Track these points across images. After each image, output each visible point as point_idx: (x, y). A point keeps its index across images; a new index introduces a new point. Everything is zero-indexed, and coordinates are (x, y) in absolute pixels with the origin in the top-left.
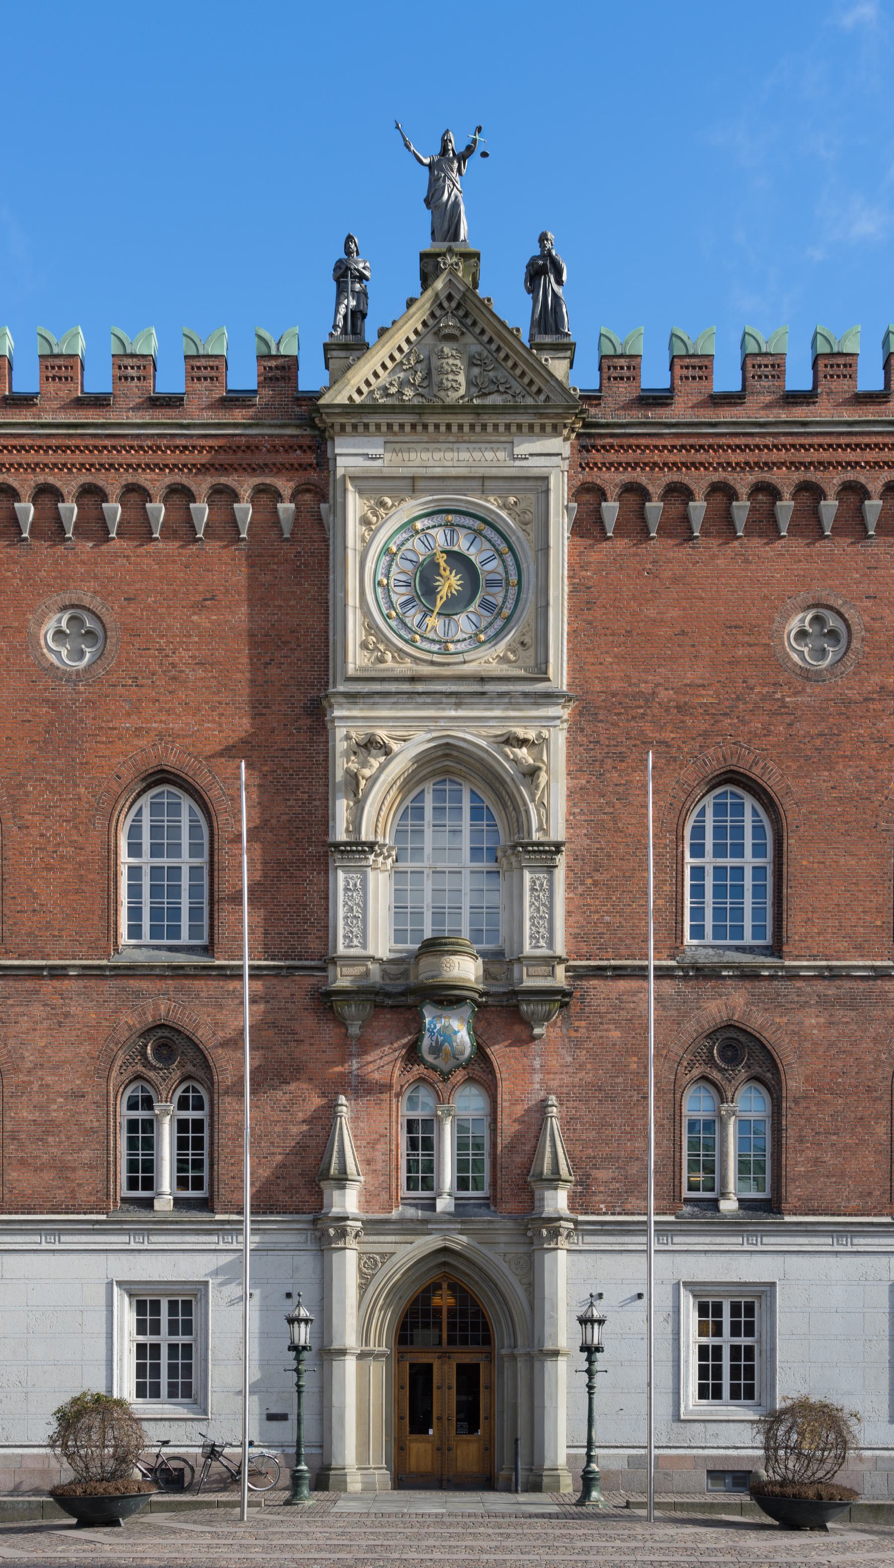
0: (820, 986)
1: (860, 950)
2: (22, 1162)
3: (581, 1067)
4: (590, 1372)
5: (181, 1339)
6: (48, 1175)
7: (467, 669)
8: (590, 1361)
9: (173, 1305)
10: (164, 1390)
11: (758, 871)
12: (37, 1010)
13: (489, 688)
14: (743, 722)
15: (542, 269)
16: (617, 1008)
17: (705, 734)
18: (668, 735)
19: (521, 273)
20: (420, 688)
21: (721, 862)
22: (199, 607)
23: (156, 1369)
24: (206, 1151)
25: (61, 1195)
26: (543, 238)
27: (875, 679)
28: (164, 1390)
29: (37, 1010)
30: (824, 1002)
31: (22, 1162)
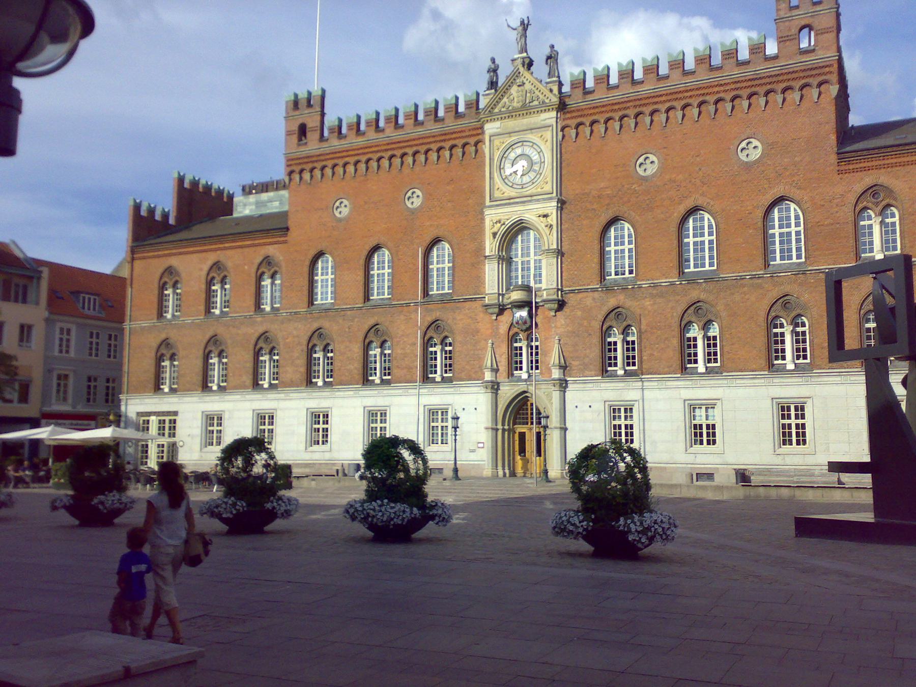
0: (651, 290)
1: (664, 275)
2: (398, 367)
3: (568, 325)
4: (456, 435)
5: (786, 421)
6: (405, 371)
7: (527, 193)
8: (456, 431)
9: (626, 410)
10: (705, 442)
11: (630, 250)
12: (402, 317)
13: (535, 198)
14: (621, 198)
15: (552, 58)
16: (579, 304)
17: (608, 204)
18: (595, 206)
19: (545, 58)
20: (512, 201)
21: (617, 248)
22: (448, 184)
23: (708, 434)
24: (718, 348)
25: (408, 377)
26: (552, 47)
27: (667, 177)
28: (705, 442)
29: (402, 317)
30: (653, 296)
31: (398, 367)
